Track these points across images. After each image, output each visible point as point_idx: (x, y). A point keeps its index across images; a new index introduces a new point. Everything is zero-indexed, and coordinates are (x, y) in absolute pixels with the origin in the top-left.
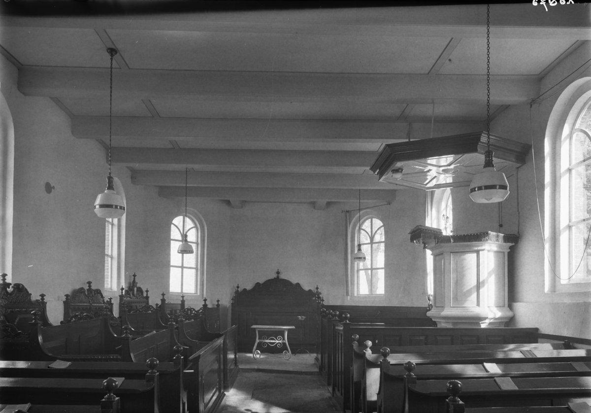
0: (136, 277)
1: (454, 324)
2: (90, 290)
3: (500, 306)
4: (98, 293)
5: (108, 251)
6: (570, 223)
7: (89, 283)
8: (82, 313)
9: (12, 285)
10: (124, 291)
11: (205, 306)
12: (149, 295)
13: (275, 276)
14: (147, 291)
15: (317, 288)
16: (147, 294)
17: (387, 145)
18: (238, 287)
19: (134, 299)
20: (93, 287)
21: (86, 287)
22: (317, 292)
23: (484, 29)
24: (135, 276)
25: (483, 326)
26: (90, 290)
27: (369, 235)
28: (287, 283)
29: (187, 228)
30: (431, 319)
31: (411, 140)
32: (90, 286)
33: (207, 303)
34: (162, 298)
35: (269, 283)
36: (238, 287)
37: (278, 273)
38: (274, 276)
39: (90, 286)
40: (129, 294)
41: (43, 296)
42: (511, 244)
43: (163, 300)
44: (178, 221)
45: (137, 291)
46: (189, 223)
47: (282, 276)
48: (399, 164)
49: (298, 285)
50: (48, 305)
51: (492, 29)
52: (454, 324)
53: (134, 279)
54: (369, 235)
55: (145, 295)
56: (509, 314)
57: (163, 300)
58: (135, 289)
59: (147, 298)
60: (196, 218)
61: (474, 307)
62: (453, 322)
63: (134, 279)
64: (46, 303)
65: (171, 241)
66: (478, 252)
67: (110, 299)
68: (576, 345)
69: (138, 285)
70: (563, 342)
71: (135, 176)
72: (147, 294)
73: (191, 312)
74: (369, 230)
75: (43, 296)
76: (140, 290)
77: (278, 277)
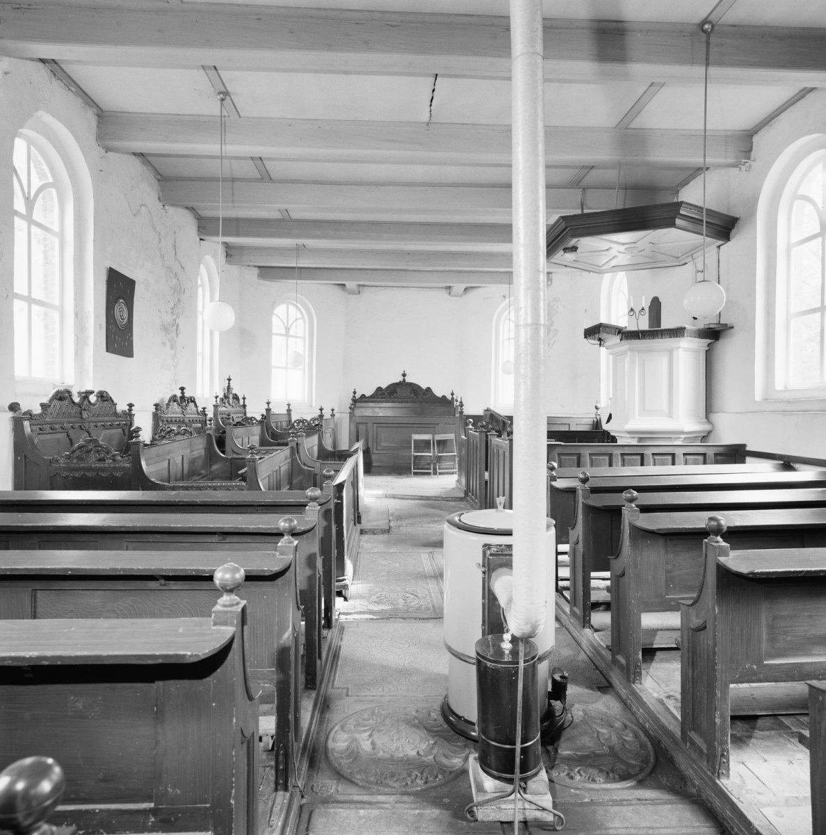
0: (231, 382)
1: (640, 439)
2: (183, 397)
4: (192, 401)
5: (199, 350)
7: (182, 389)
8: (179, 427)
9: (95, 393)
10: (218, 399)
12: (291, 408)
13: (401, 379)
14: (244, 399)
15: (452, 394)
17: (562, 217)
18: (355, 393)
19: (230, 409)
20: (187, 394)
21: (179, 394)
22: (453, 398)
23: (699, 70)
26: (183, 397)
27: (284, 323)
29: (292, 319)
30: (608, 433)
31: (586, 211)
32: (183, 393)
34: (267, 407)
36: (355, 393)
37: (404, 375)
38: (399, 379)
39: (183, 393)
40: (224, 403)
41: (131, 405)
42: (709, 341)
43: (268, 410)
44: (281, 310)
45: (233, 398)
47: (408, 380)
48: (573, 242)
49: (429, 389)
50: (135, 418)
51: (713, 70)
52: (640, 439)
53: (229, 384)
54: (284, 323)
55: (241, 403)
56: (707, 427)
57: (268, 410)
58: (231, 396)
59: (244, 406)
62: (639, 438)
63: (229, 384)
65: (273, 336)
66: (671, 352)
67: (204, 408)
68: (797, 466)
69: (234, 392)
70: (782, 462)
71: (231, 253)
73: (303, 423)
74: (284, 317)
75: (131, 405)
76: (236, 397)
77: (404, 380)
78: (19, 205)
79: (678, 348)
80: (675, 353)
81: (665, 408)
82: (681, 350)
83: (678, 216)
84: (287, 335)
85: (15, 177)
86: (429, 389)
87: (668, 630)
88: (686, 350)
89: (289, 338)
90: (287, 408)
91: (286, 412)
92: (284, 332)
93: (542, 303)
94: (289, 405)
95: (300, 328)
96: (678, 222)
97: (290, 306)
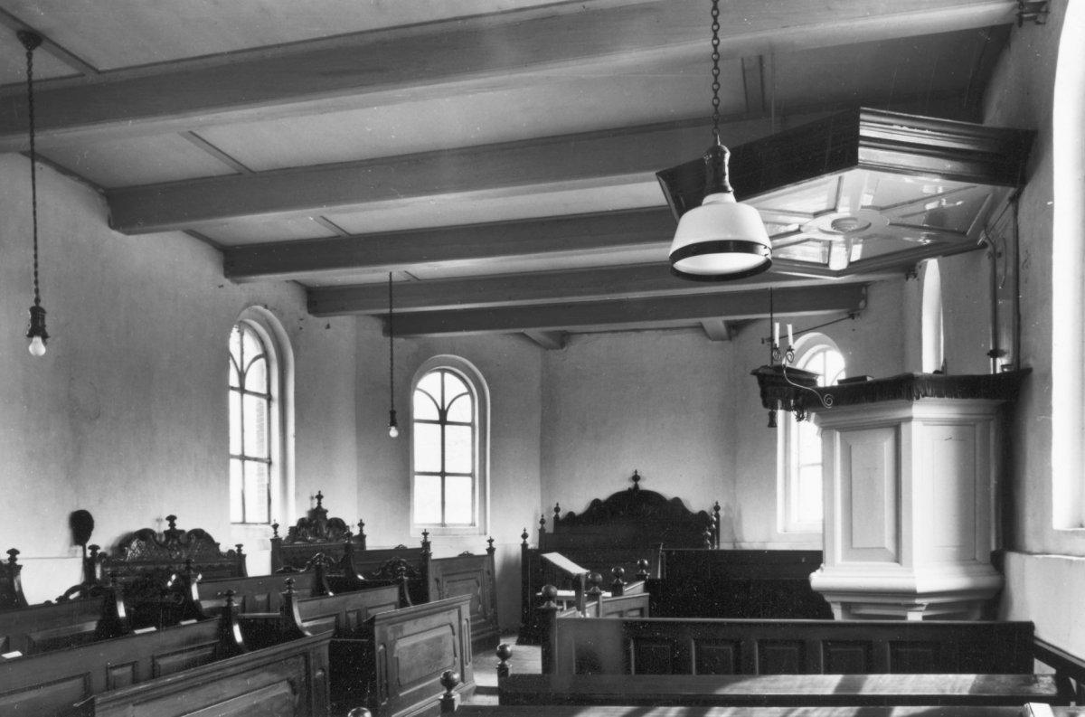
3: (965, 557)
6: (763, 247)
11: (524, 546)
12: (365, 532)
16: (361, 531)
18: (557, 510)
24: (320, 497)
25: (915, 617)
27: (236, 367)
28: (653, 498)
33: (528, 540)
35: (617, 498)
36: (557, 510)
37: (636, 478)
38: (626, 485)
46: (454, 385)
47: (645, 485)
54: (236, 367)
56: (986, 581)
60: (465, 375)
61: (598, 606)
64: (20, 567)
66: (896, 427)
72: (361, 531)
75: (13, 553)
77: (636, 487)
78: (234, 380)
79: (909, 419)
80: (904, 427)
81: (889, 544)
82: (914, 424)
83: (861, 142)
84: (443, 421)
85: (231, 361)
86: (218, 544)
87: (416, 634)
88: (926, 421)
89: (447, 427)
90: (522, 541)
91: (486, 553)
92: (436, 417)
93: (975, 222)
94: (425, 534)
95: (462, 410)
96: (864, 154)
97: (448, 376)
